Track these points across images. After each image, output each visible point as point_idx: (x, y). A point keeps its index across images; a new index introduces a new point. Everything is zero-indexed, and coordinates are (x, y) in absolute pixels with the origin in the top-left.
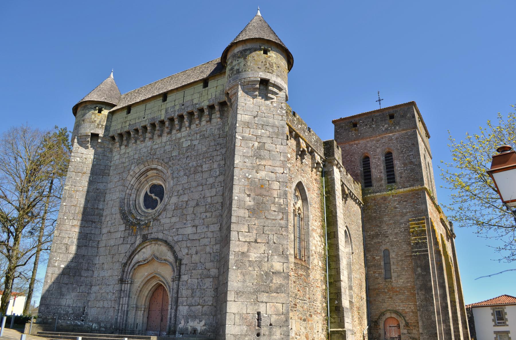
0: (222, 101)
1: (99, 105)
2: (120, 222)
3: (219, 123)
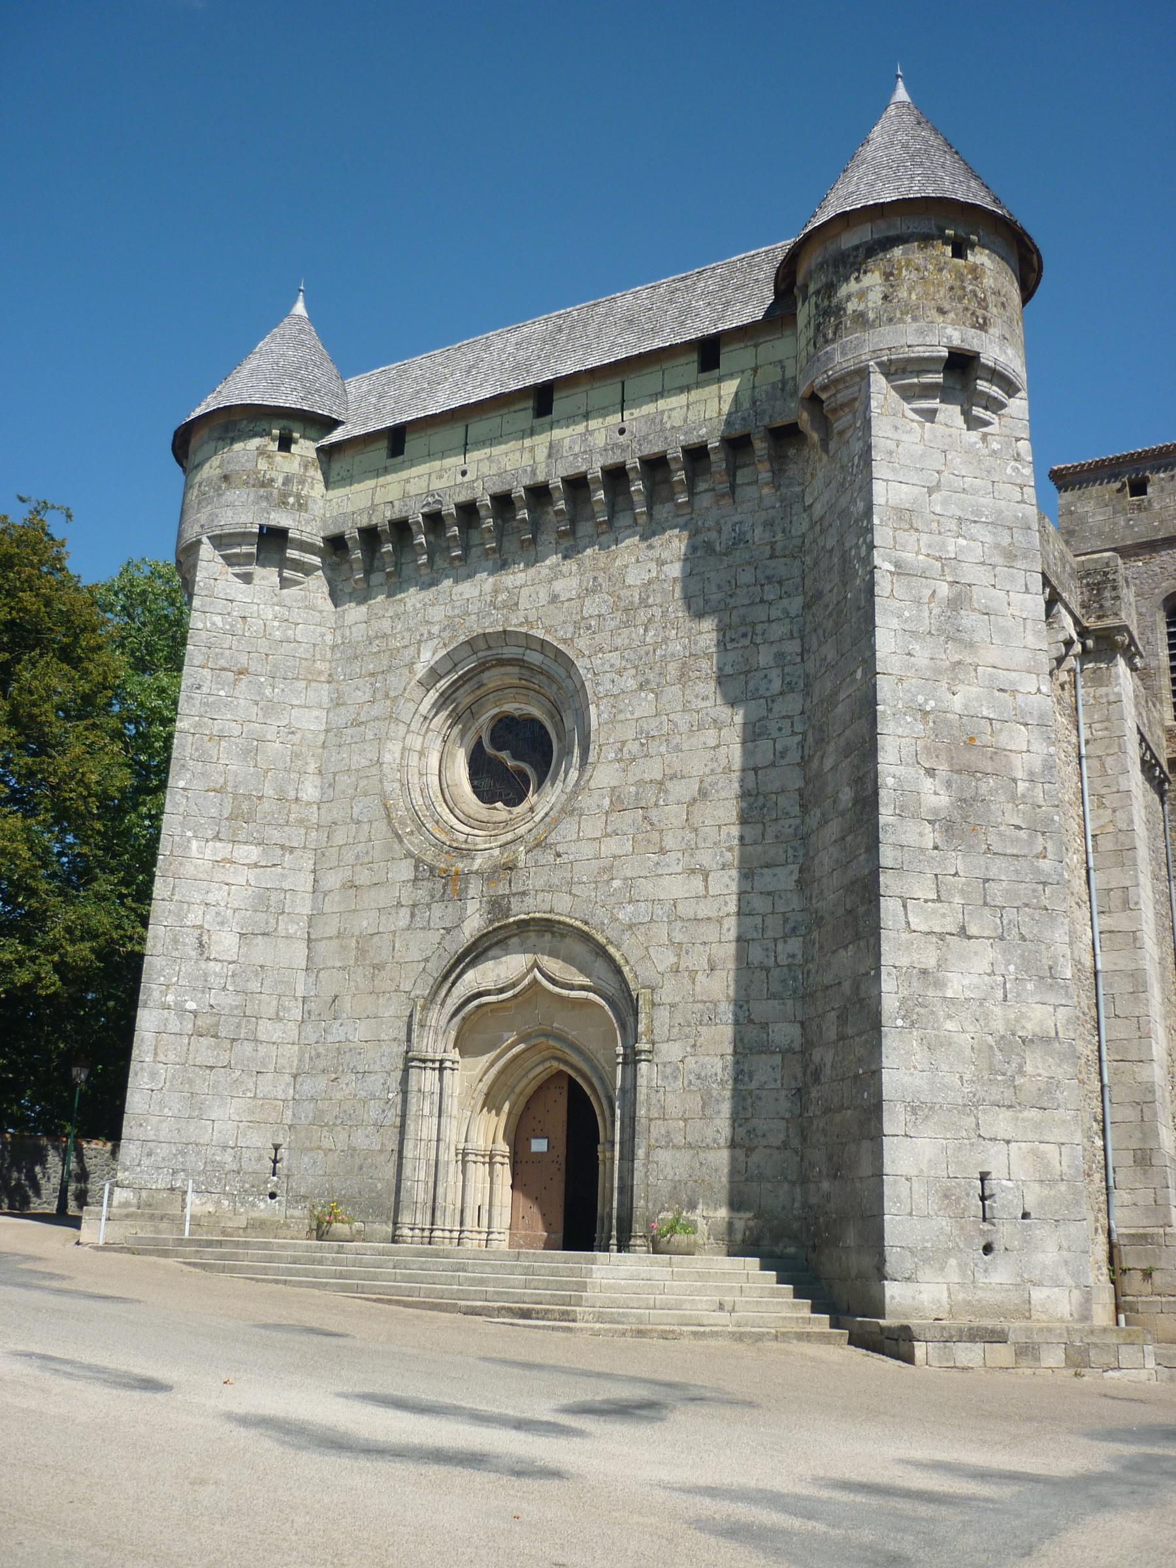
0: (779, 422)
2: (391, 849)
3: (767, 502)
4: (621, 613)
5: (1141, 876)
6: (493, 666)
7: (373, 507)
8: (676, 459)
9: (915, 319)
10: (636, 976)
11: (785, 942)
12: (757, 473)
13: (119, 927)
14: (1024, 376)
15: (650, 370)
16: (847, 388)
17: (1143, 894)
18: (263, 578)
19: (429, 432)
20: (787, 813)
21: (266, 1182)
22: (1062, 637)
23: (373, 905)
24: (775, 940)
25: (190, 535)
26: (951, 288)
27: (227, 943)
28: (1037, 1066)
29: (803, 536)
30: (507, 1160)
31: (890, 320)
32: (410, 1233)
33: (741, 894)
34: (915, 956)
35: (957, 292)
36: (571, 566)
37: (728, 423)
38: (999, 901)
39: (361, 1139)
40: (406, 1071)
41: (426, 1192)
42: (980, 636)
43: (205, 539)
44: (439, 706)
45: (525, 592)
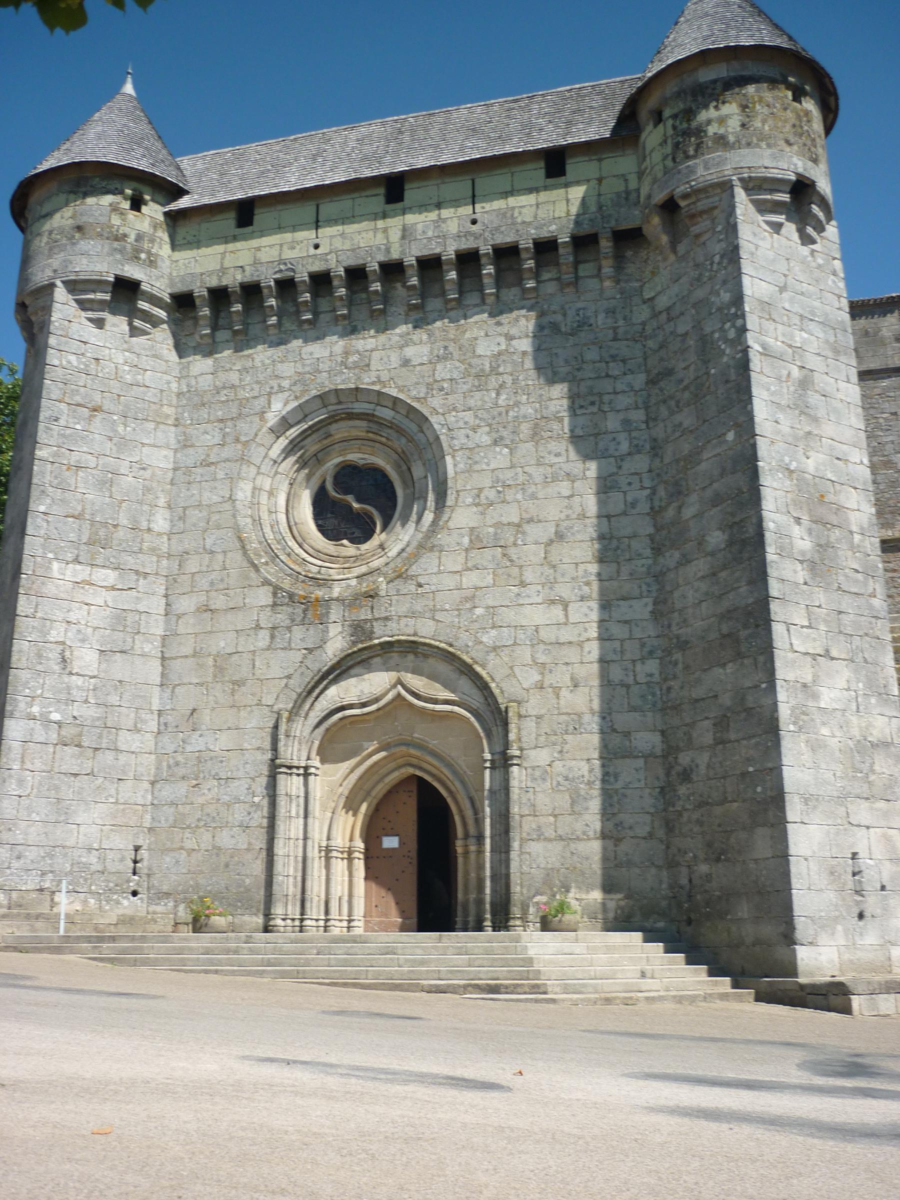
0: (624, 226)
1: (135, 185)
2: (247, 578)
6: (342, 419)
7: (223, 270)
8: (527, 249)
9: (769, 146)
10: (502, 692)
11: (643, 663)
15: (499, 172)
16: (708, 197)
18: (114, 325)
19: (279, 207)
20: (639, 555)
21: (128, 881)
23: (230, 627)
24: (634, 661)
26: (794, 126)
27: (88, 659)
29: (644, 324)
30: (362, 856)
31: (749, 144)
32: (282, 923)
33: (601, 622)
36: (421, 335)
37: (577, 223)
38: (849, 630)
39: (225, 839)
41: (295, 886)
42: (821, 413)
44: (288, 451)
45: (376, 355)
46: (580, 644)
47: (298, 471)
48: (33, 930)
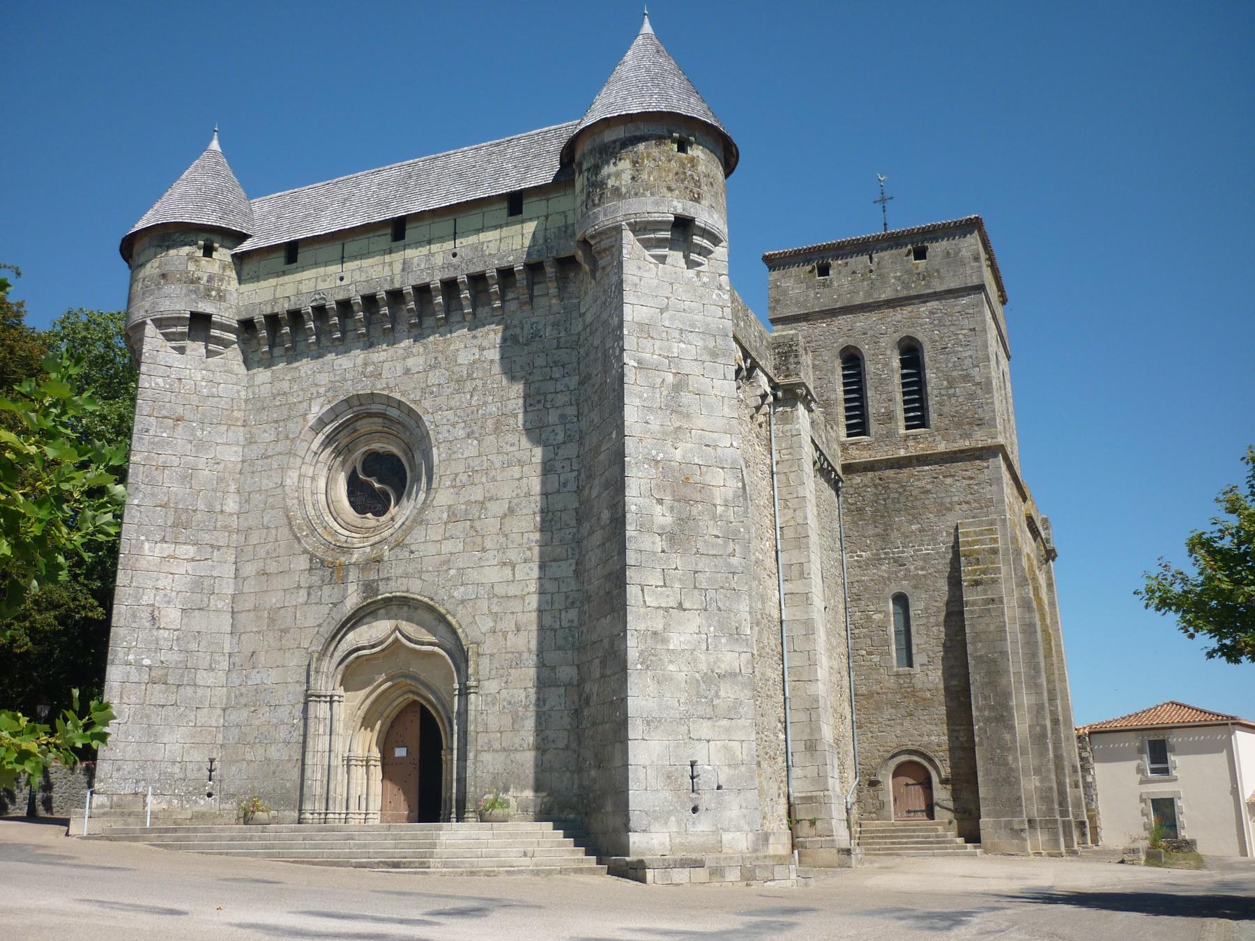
0: (563, 255)
1: (206, 236)
2: (292, 547)
3: (555, 309)
4: (458, 383)
5: (812, 556)
7: (275, 300)
9: (652, 194)
12: (548, 289)
13: (75, 599)
14: (726, 231)
17: (813, 567)
22: (759, 392)
23: (280, 587)
25: (137, 317)
28: (728, 692)
29: (579, 334)
31: (636, 194)
34: (649, 623)
35: (680, 176)
36: (418, 348)
37: (528, 254)
39: (273, 752)
40: (306, 703)
41: (322, 787)
43: (149, 321)
46: (523, 598)
47: (335, 458)
48: (126, 823)
